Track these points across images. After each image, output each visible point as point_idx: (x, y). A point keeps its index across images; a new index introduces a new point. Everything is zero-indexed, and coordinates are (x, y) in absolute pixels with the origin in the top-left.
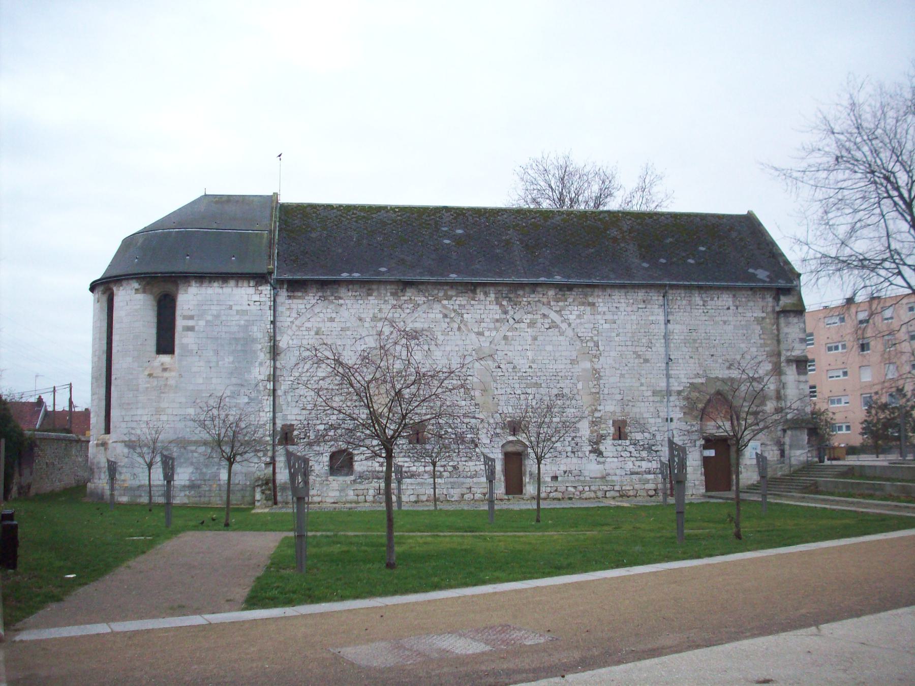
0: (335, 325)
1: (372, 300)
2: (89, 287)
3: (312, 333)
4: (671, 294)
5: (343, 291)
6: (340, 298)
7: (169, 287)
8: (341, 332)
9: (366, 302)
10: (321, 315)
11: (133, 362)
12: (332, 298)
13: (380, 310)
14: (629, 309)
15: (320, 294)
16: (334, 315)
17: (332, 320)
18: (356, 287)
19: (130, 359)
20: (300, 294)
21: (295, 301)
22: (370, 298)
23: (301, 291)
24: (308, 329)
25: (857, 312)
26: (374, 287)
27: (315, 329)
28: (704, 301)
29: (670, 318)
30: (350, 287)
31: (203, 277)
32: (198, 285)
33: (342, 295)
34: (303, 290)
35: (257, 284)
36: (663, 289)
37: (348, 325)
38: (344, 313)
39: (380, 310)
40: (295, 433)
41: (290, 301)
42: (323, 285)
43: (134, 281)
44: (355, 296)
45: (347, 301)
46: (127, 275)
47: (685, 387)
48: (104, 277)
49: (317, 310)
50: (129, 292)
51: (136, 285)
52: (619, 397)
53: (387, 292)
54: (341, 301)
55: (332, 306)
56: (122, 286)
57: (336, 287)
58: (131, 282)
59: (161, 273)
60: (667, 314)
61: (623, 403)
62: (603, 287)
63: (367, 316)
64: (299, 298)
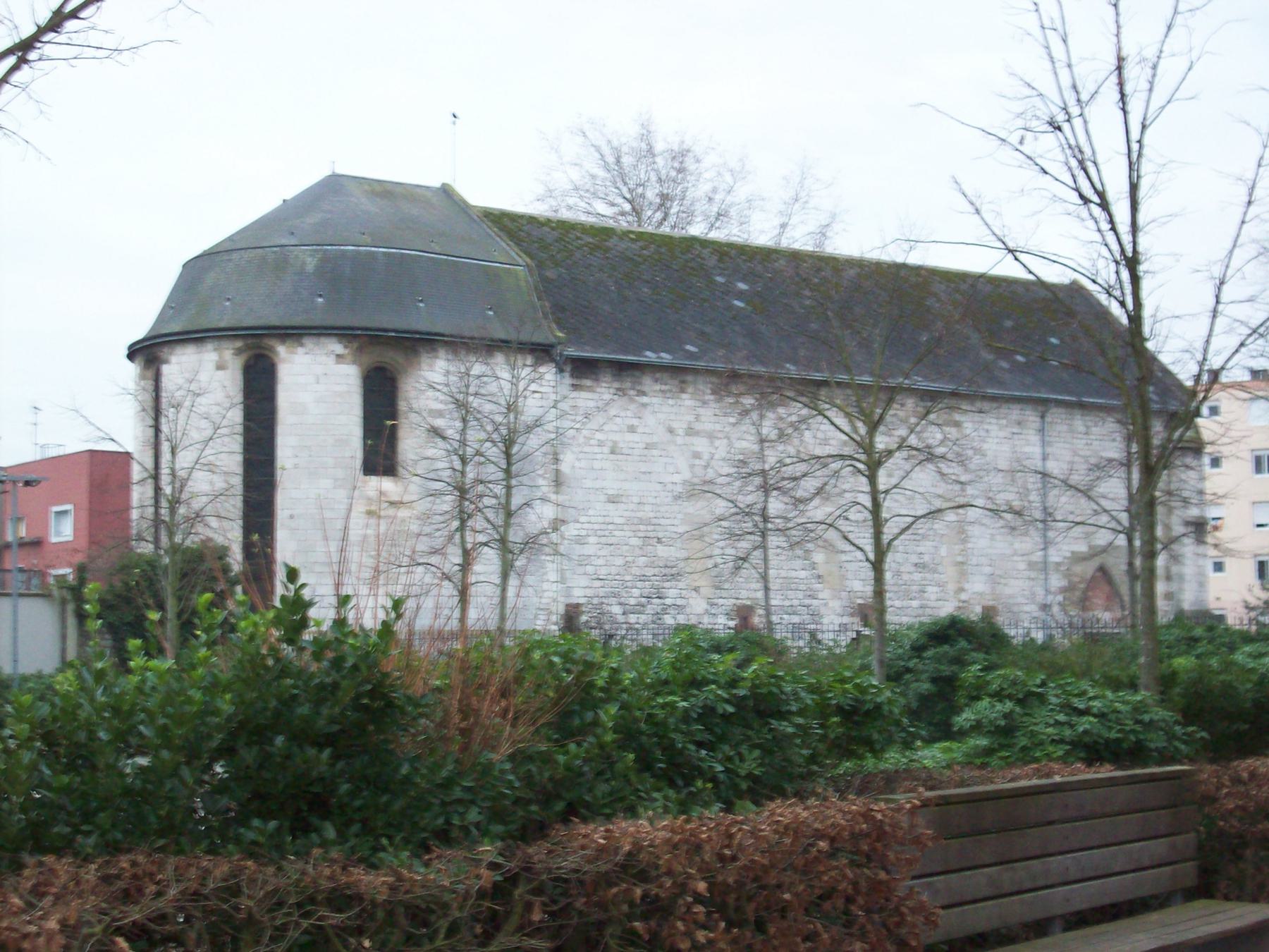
0: (635, 437)
1: (687, 400)
2: (127, 352)
3: (606, 450)
4: (1055, 414)
5: (648, 383)
6: (643, 393)
7: (390, 357)
8: (646, 452)
9: (679, 402)
10: (618, 420)
11: (335, 488)
12: (632, 392)
13: (697, 418)
14: (1002, 434)
15: (616, 385)
16: (635, 422)
17: (632, 429)
18: (665, 376)
19: (326, 483)
20: (588, 382)
21: (584, 394)
22: (684, 396)
23: (591, 379)
24: (601, 444)
25: (840, 516)
26: (689, 378)
27: (610, 444)
28: (1087, 427)
29: (1049, 450)
30: (658, 375)
31: (458, 344)
32: (450, 357)
33: (645, 389)
34: (594, 377)
35: (538, 362)
36: (1043, 405)
37: (655, 439)
38: (650, 420)
39: (697, 418)
40: (584, 618)
41: (575, 394)
42: (622, 369)
43: (334, 340)
44: (663, 391)
45: (655, 400)
46: (326, 328)
47: (1065, 558)
48: (154, 333)
49: (613, 412)
50: (324, 358)
51: (338, 348)
52: (988, 570)
53: (704, 387)
54: (645, 399)
55: (633, 407)
56: (302, 345)
57: (637, 373)
58: (323, 340)
59: (394, 331)
60: (1044, 443)
61: (993, 579)
62: (970, 398)
63: (680, 426)
64: (590, 389)
